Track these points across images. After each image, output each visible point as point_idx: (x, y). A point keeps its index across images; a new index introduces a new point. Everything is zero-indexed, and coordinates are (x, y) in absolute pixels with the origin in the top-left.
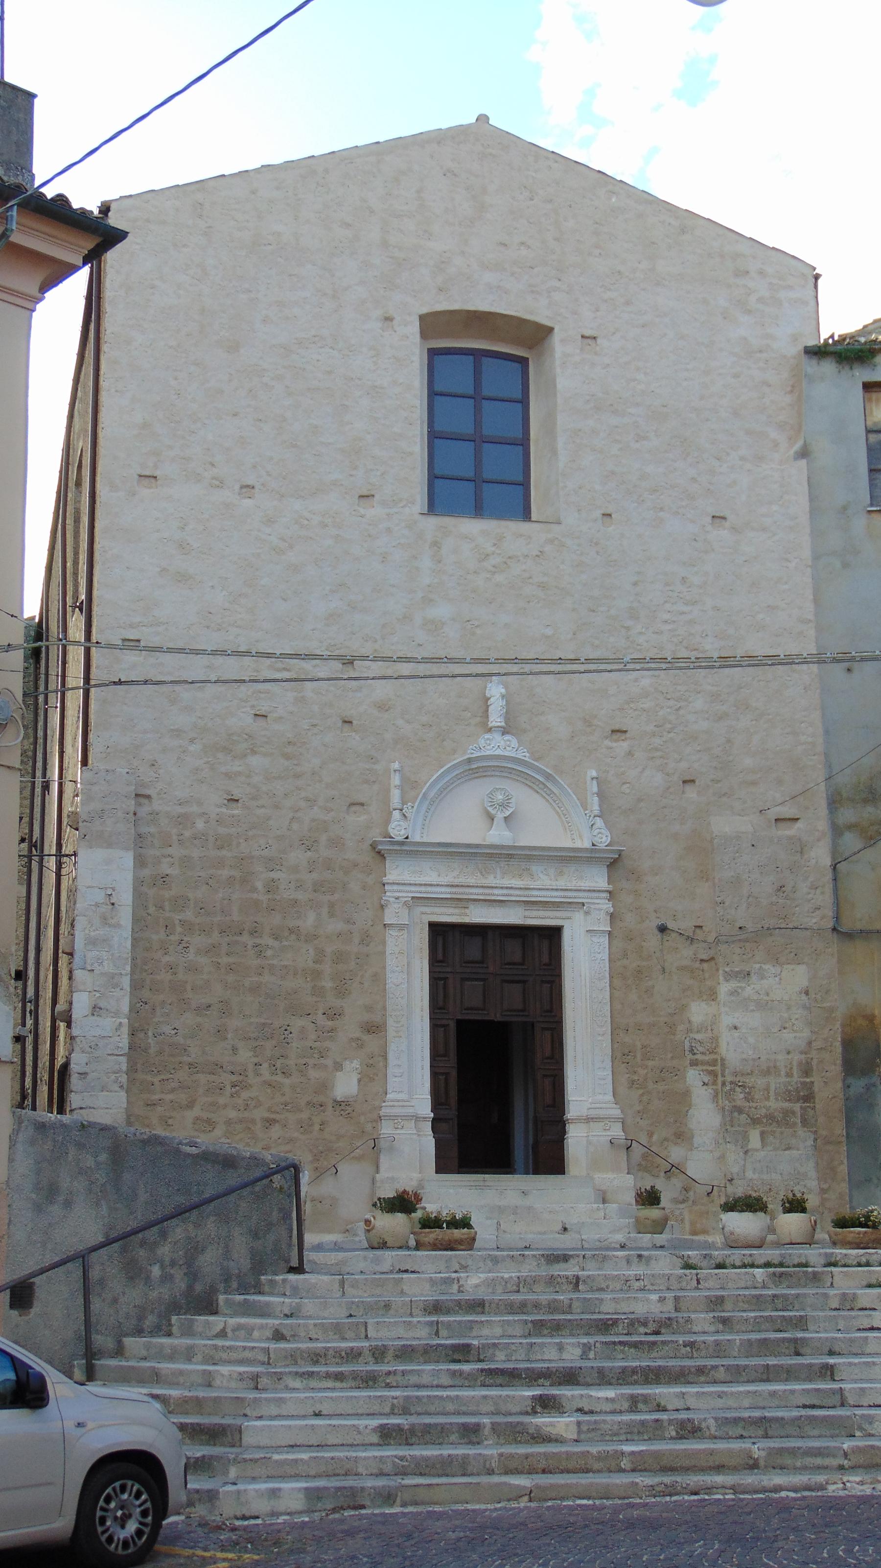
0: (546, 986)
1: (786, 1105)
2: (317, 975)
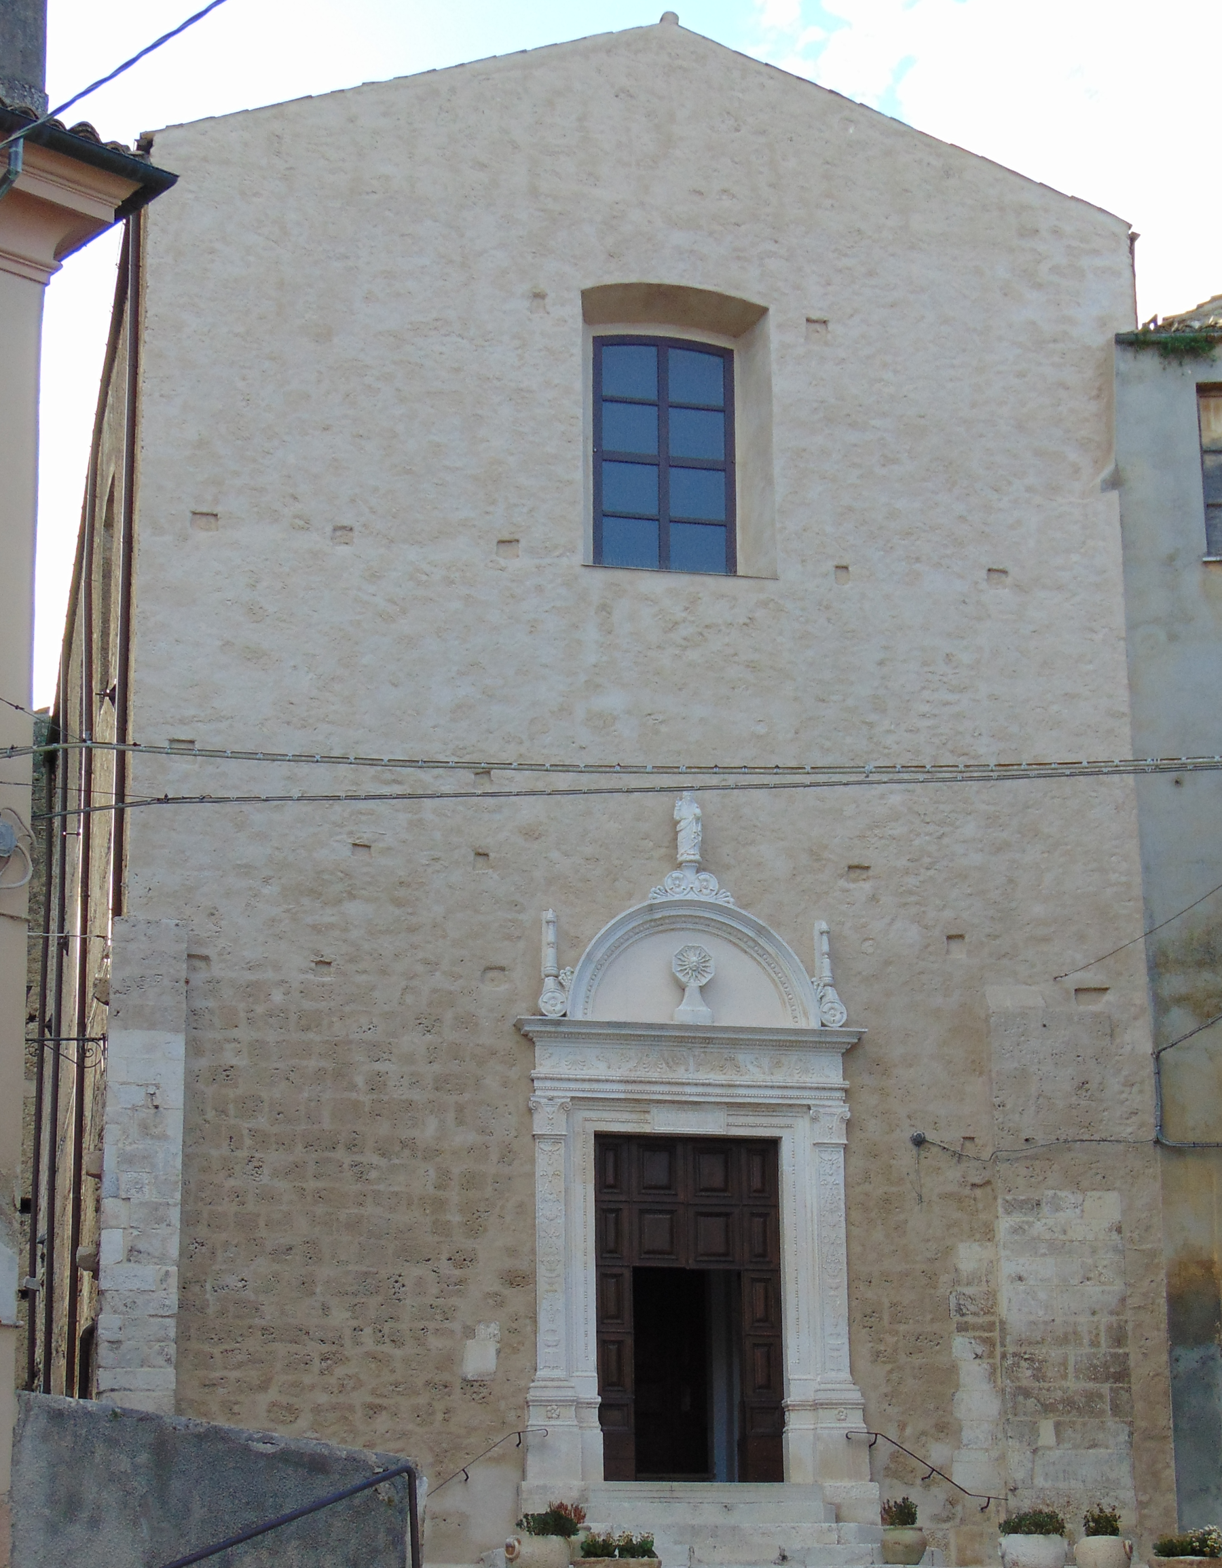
0: (758, 1221)
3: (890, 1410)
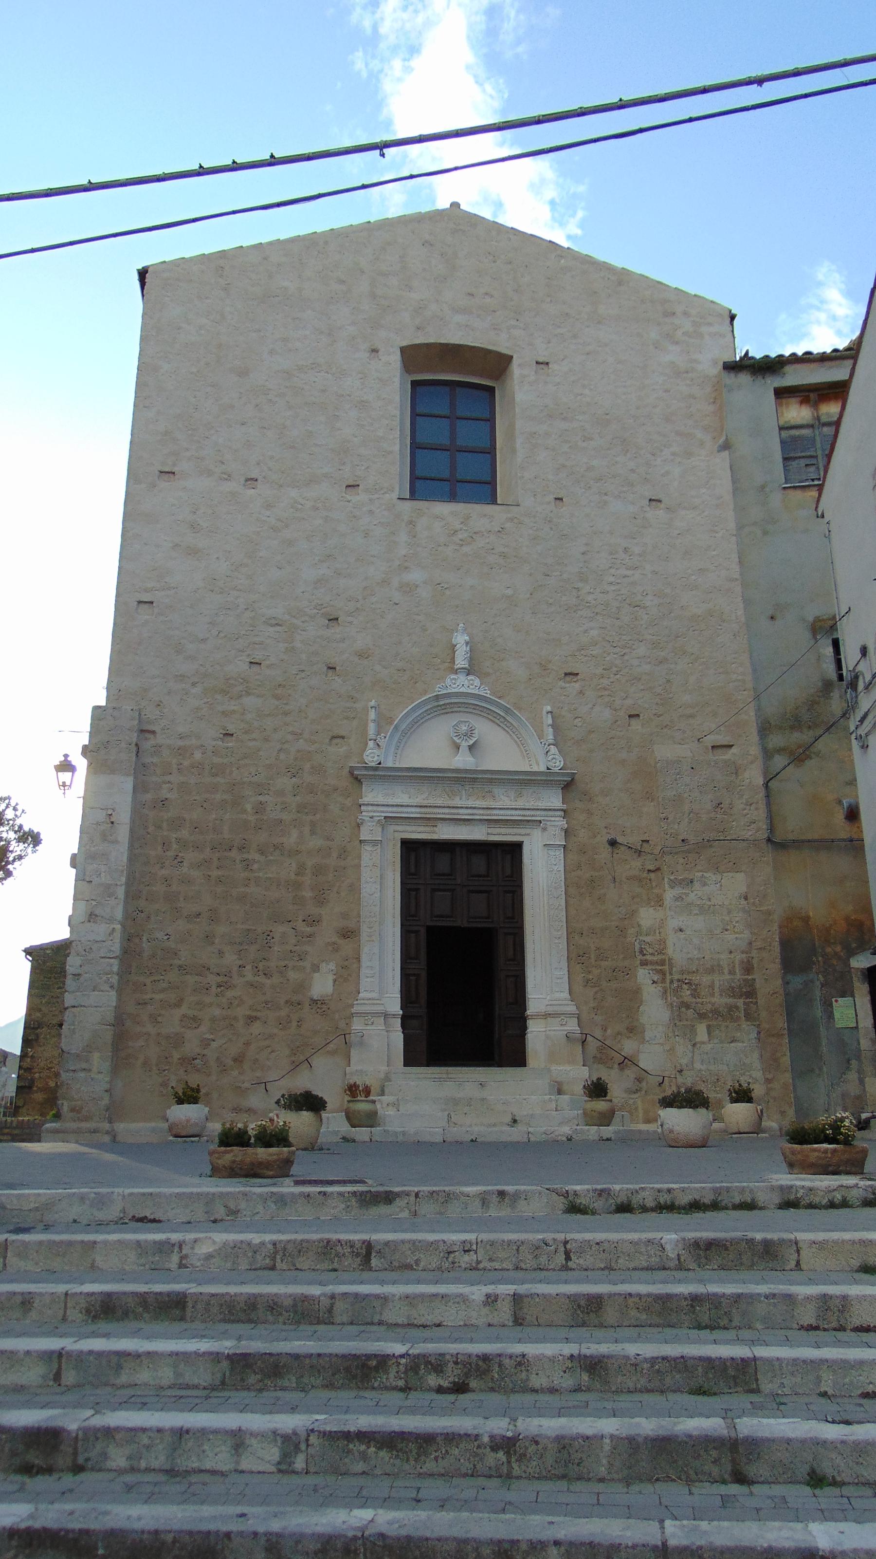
1: (730, 1001)
2: (298, 886)
3: (596, 1017)
